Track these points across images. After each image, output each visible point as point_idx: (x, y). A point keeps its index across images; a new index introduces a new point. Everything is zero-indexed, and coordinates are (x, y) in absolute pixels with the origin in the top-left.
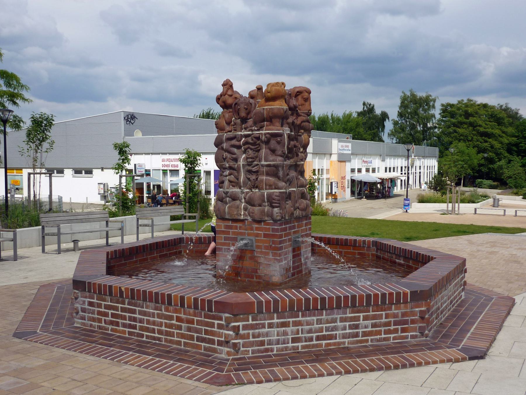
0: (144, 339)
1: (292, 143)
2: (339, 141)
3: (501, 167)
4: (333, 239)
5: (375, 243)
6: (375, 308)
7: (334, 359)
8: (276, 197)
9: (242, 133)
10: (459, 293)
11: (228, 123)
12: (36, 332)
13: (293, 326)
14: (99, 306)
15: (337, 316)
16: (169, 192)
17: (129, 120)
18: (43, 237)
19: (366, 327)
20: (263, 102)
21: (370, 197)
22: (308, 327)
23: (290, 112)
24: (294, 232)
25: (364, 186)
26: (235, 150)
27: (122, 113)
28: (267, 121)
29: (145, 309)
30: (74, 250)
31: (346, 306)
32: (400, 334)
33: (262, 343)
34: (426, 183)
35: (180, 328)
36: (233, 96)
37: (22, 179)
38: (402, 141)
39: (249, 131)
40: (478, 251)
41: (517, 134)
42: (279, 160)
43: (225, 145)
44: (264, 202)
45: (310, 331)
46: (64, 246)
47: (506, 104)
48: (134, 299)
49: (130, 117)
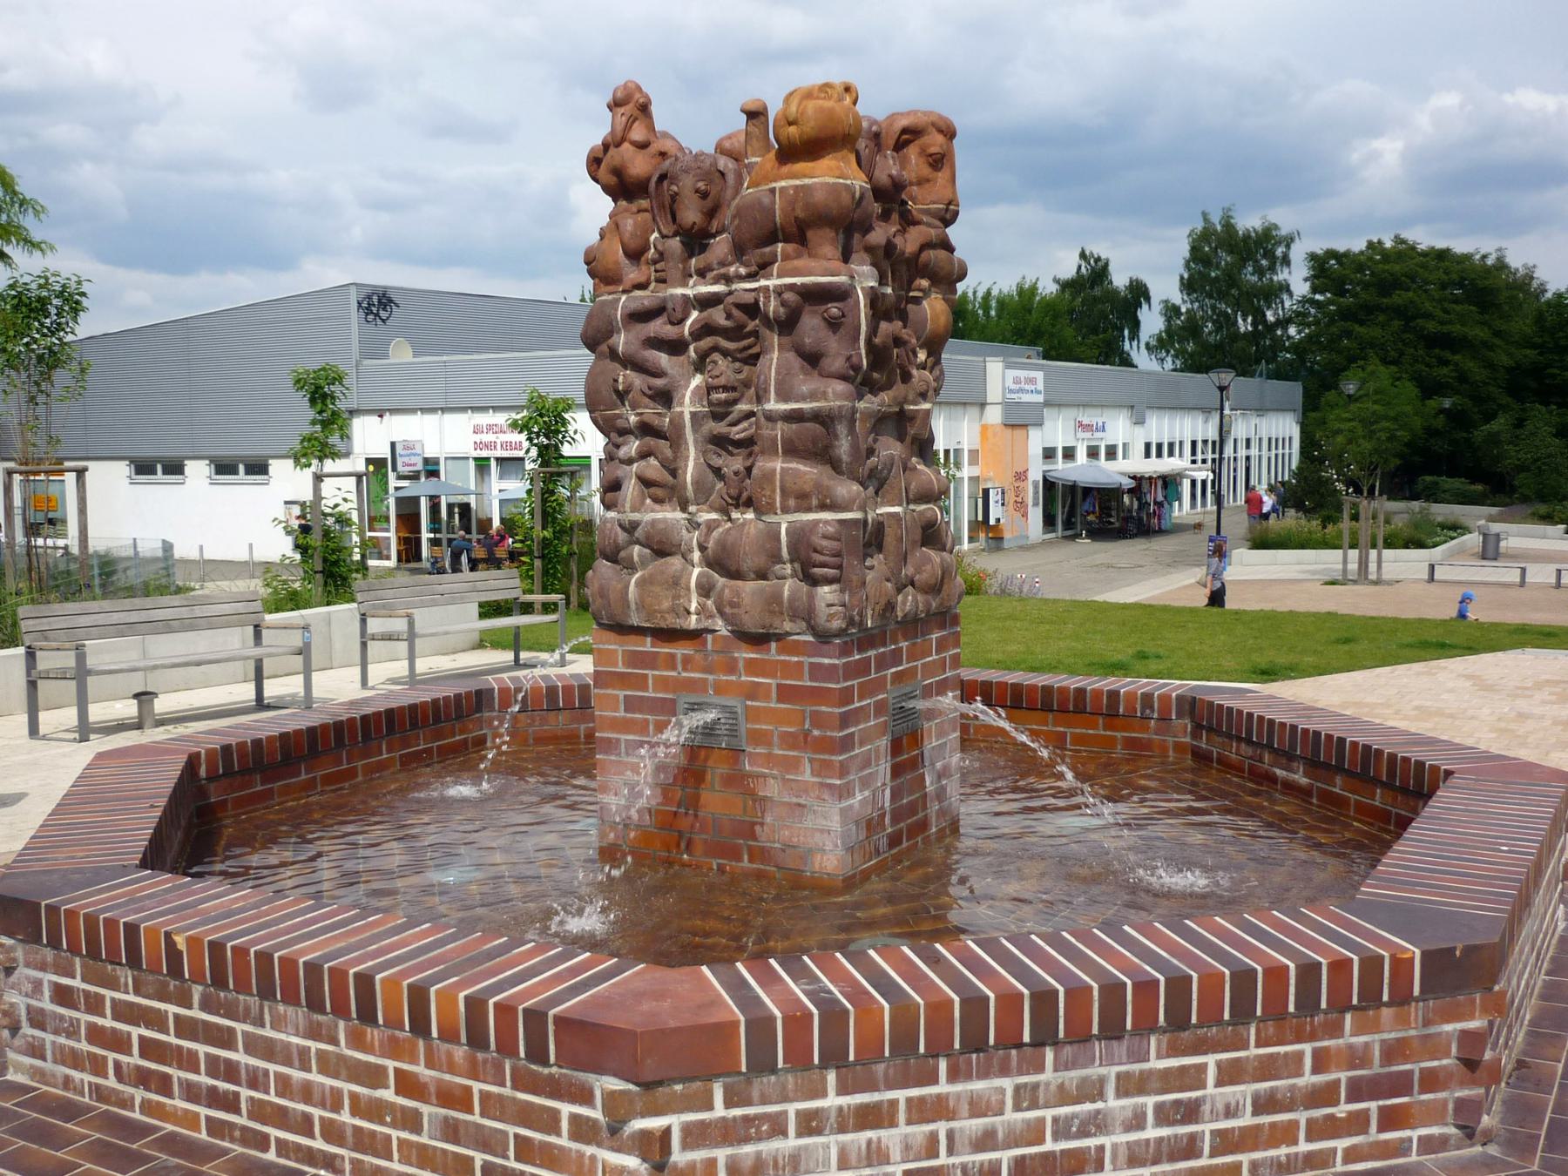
1: (884, 326)
2: (1008, 366)
3: (1494, 439)
4: (1033, 688)
5: (1190, 705)
6: (1271, 1028)
8: (825, 543)
9: (689, 292)
11: (635, 255)
13: (909, 1122)
14: (95, 1005)
15: (1103, 1071)
16: (496, 523)
17: (374, 310)
19: (1230, 1113)
20: (769, 166)
21: (1100, 533)
22: (977, 1124)
23: (877, 208)
24: (898, 677)
25: (1084, 499)
26: (663, 359)
27: (353, 290)
28: (786, 241)
29: (268, 1032)
31: (1146, 1025)
32: (1374, 1135)
35: (411, 1121)
36: (656, 146)
37: (63, 493)
38: (1196, 364)
39: (716, 281)
40: (1522, 716)
41: (1538, 340)
42: (834, 395)
43: (621, 341)
44: (780, 561)
46: (97, 712)
47: (1500, 250)
48: (225, 986)
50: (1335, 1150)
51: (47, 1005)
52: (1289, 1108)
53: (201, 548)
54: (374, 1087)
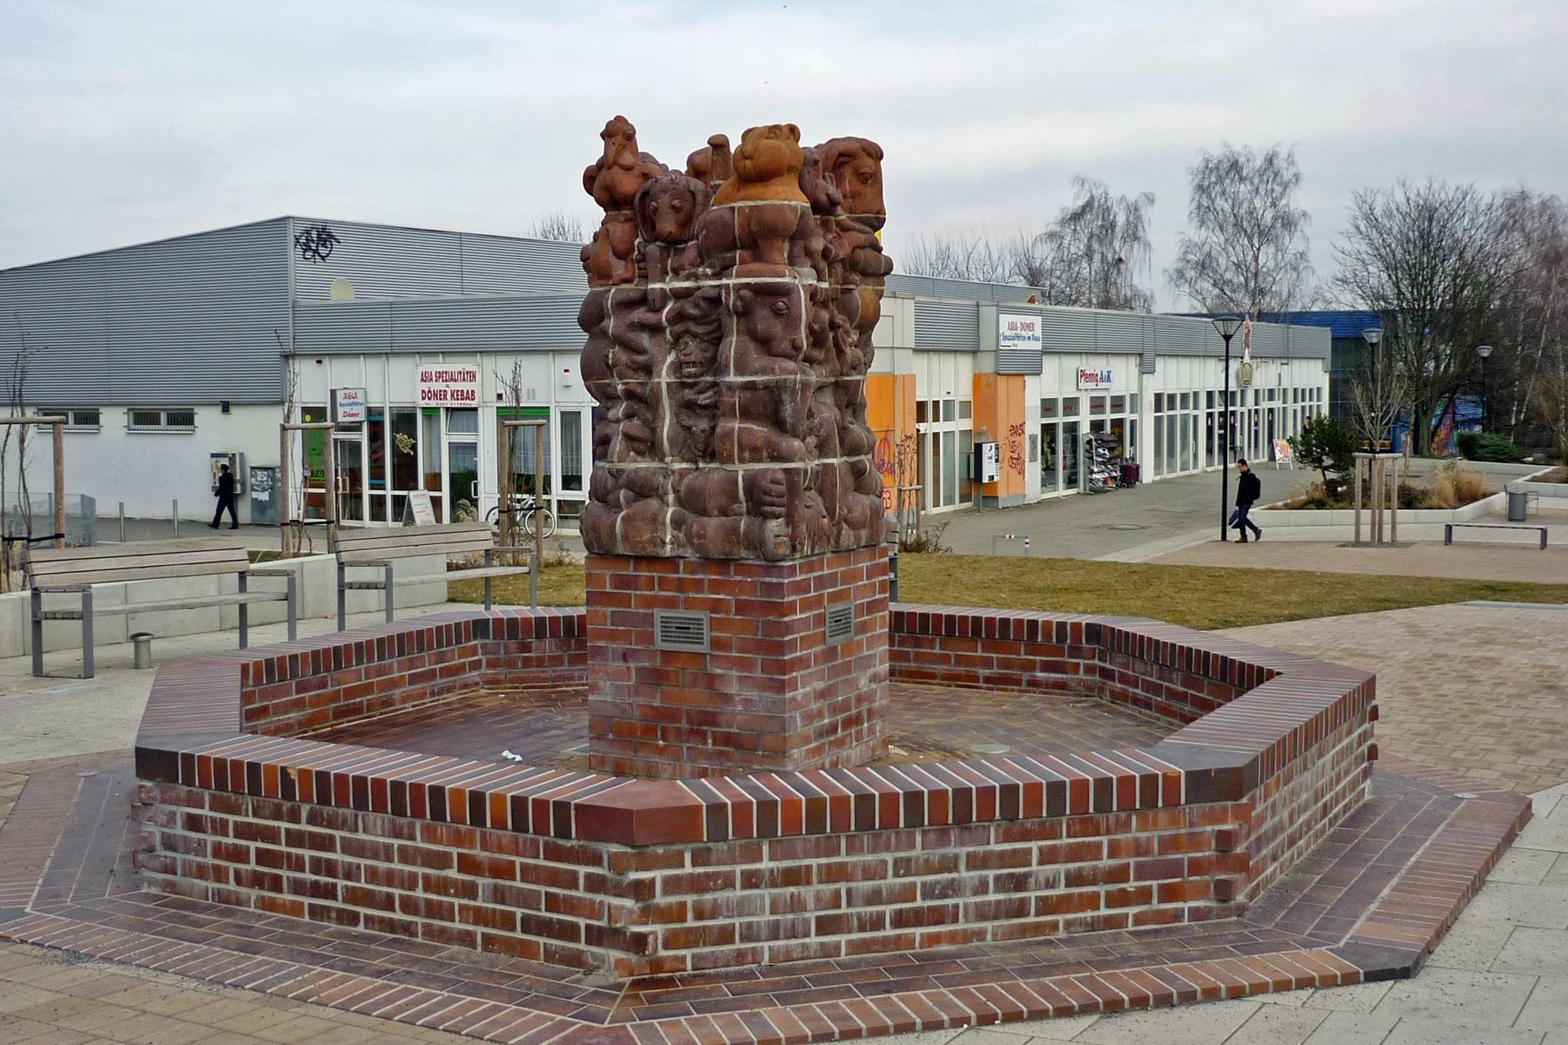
0: (361, 928)
7: (947, 982)
9: (667, 287)
10: (1354, 784)
11: (622, 255)
12: (22, 913)
13: (820, 882)
14: (220, 828)
15: (957, 850)
17: (313, 246)
18: (37, 624)
19: (1050, 884)
26: (645, 340)
28: (742, 248)
30: (137, 666)
32: (1156, 905)
33: (726, 935)
34: (1291, 441)
35: (470, 891)
39: (687, 278)
43: (611, 324)
45: (874, 897)
49: (314, 235)
50: (1127, 915)
51: (179, 831)
52: (1094, 883)
53: (121, 505)
54: (442, 868)
